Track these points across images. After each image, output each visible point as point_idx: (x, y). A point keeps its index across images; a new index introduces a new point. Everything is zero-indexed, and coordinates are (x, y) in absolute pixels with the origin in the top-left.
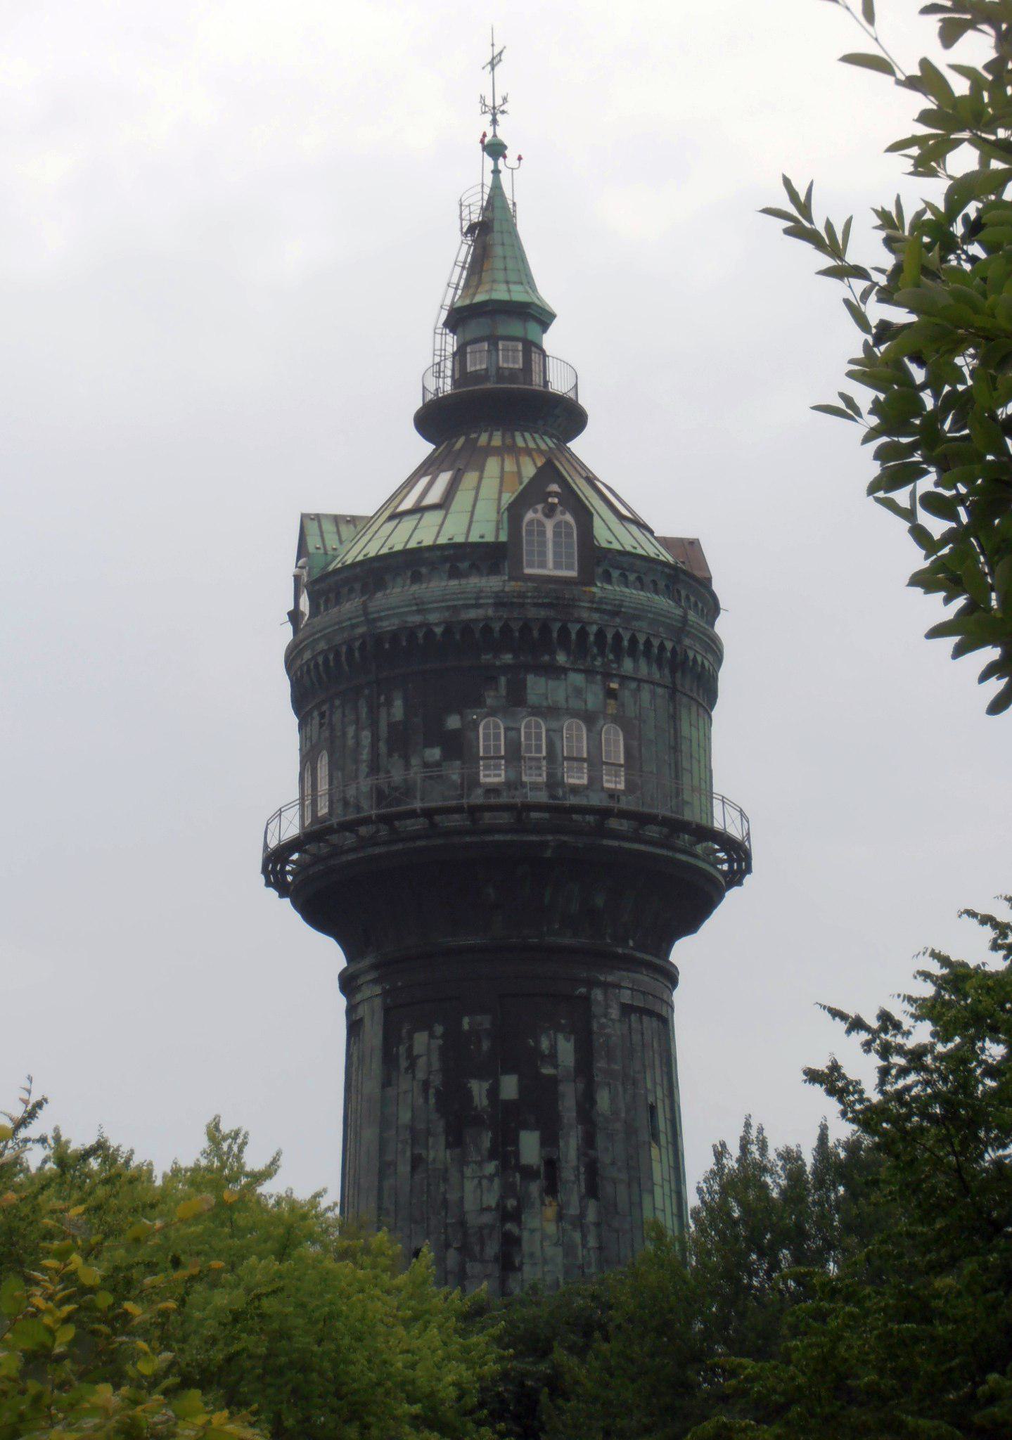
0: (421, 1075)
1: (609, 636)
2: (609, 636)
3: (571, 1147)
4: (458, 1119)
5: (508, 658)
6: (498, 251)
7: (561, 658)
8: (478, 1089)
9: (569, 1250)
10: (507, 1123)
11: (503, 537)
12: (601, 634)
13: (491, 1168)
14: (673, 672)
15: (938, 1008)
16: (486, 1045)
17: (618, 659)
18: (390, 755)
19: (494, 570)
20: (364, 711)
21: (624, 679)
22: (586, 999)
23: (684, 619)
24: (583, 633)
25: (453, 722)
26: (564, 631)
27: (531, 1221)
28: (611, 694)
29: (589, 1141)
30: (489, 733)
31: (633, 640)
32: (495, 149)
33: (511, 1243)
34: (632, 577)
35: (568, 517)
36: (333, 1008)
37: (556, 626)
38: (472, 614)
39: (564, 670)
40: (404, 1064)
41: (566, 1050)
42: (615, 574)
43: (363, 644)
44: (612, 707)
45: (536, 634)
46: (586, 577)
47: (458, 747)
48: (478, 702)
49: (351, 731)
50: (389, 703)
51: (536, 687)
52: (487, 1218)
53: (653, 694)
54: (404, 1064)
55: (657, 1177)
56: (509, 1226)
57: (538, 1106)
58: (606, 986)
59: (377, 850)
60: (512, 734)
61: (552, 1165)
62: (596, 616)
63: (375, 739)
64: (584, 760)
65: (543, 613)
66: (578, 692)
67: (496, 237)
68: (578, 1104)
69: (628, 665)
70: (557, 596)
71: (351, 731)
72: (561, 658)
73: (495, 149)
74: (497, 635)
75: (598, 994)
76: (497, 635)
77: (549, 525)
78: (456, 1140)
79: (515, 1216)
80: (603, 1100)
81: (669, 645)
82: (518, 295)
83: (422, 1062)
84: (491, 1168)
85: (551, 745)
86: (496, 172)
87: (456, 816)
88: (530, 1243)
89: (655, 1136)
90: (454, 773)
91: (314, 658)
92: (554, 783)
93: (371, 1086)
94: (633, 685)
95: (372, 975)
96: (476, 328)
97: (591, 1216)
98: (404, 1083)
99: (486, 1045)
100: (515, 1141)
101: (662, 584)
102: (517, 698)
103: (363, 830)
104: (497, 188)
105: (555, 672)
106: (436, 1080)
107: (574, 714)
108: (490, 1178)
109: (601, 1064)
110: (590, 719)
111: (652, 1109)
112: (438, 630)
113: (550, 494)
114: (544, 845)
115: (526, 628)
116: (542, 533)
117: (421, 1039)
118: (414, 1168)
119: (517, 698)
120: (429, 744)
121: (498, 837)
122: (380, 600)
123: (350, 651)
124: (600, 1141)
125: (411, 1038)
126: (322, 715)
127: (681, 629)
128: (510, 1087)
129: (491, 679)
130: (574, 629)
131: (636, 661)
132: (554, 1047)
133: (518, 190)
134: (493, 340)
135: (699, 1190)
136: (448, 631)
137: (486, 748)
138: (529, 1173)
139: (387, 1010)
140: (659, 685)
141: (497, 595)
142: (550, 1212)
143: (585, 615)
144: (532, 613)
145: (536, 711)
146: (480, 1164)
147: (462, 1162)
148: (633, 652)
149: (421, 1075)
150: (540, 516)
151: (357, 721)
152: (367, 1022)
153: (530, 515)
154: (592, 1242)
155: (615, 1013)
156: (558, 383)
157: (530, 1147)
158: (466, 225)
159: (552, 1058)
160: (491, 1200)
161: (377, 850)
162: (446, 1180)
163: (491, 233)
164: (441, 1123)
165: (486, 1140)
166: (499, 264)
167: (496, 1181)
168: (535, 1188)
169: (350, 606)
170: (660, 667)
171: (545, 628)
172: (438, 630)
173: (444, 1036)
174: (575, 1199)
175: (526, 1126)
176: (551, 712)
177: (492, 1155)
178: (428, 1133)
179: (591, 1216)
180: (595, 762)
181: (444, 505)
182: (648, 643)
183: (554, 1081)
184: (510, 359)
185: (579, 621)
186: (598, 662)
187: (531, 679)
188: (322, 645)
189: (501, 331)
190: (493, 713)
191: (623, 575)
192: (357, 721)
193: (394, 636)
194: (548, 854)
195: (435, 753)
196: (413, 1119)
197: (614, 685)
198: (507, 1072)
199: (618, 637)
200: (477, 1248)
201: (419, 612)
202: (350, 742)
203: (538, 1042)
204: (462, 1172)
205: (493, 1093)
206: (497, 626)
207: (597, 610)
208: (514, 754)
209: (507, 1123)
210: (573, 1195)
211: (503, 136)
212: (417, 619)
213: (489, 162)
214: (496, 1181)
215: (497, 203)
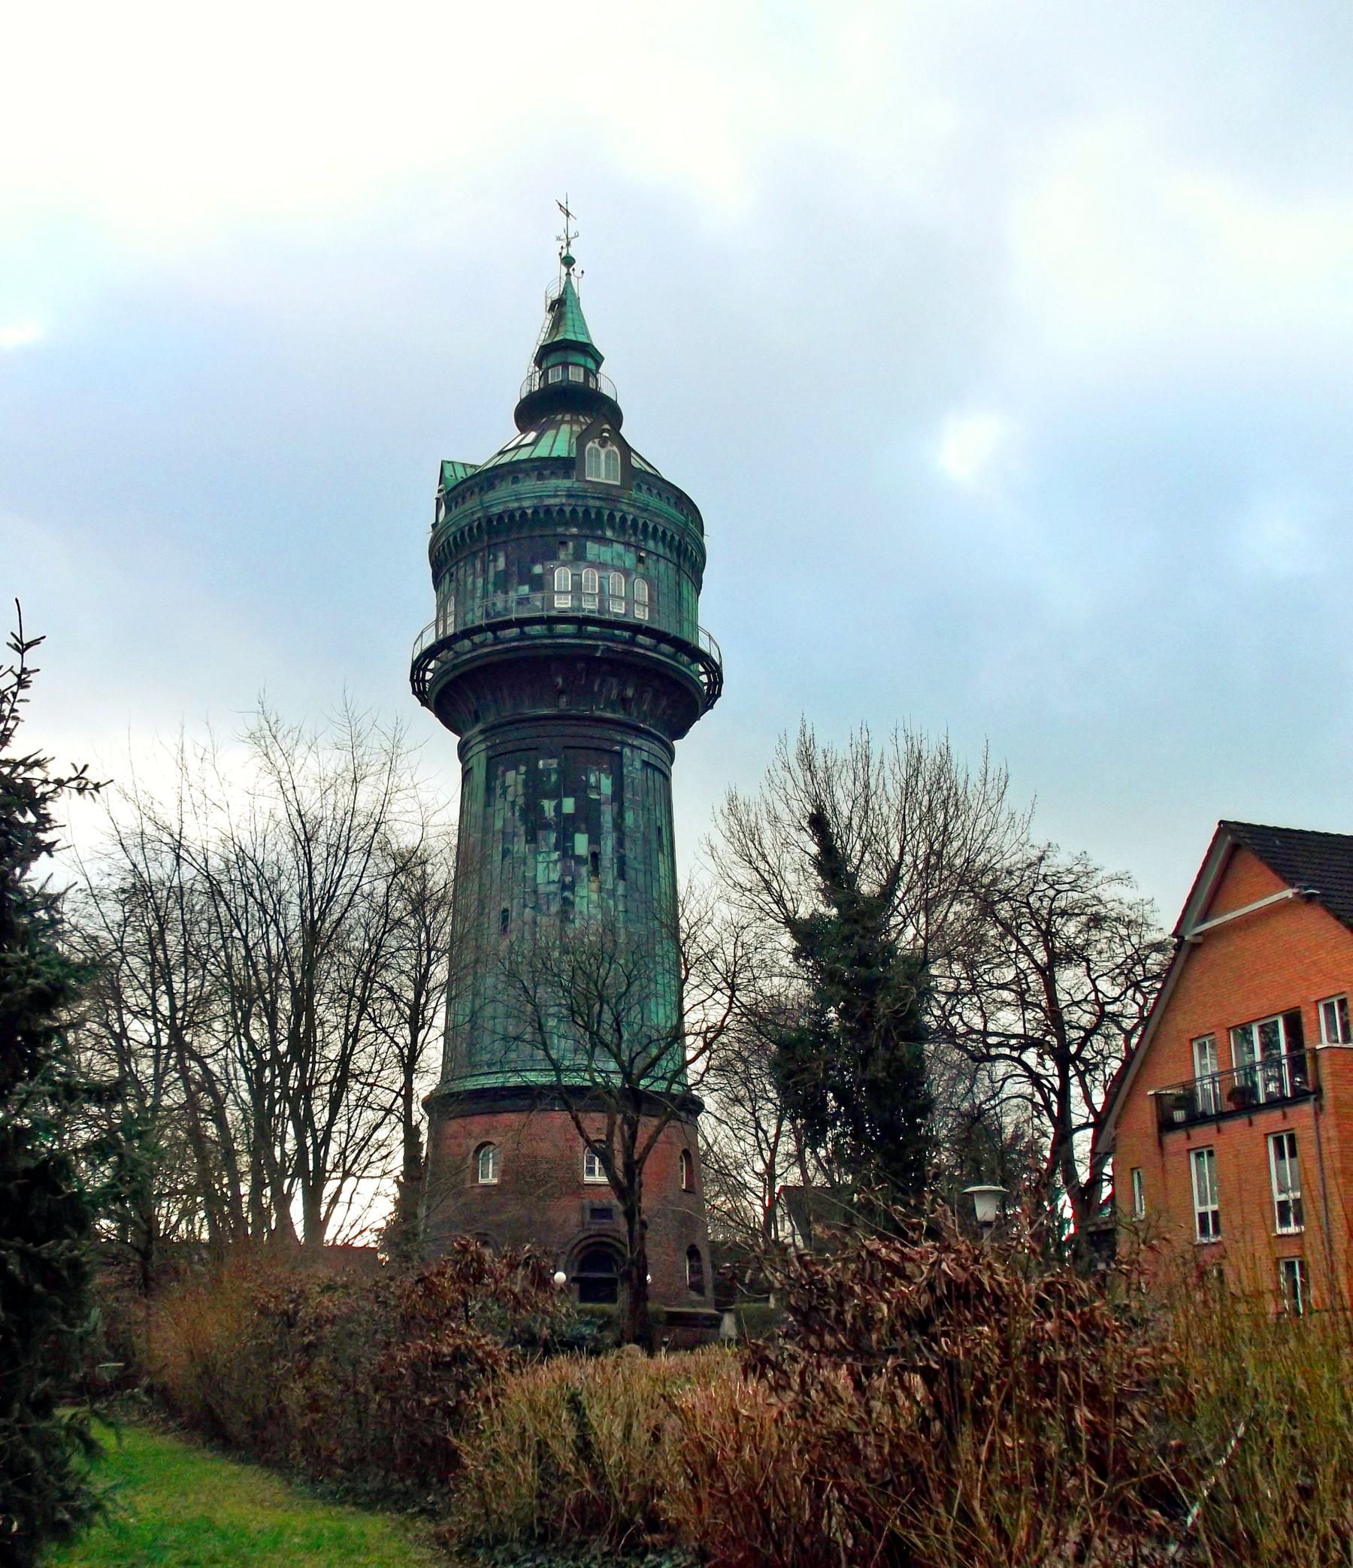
0: (510, 798)
1: (640, 522)
2: (640, 522)
3: (608, 845)
4: (534, 824)
6: (569, 315)
7: (609, 534)
8: (549, 806)
9: (605, 912)
10: (566, 828)
11: (573, 455)
12: (635, 521)
13: (555, 856)
14: (679, 556)
16: (554, 778)
17: (645, 539)
18: (495, 592)
19: (567, 475)
20: (479, 566)
21: (649, 552)
22: (620, 754)
23: (687, 524)
24: (623, 519)
25: (538, 569)
26: (611, 516)
27: (581, 891)
28: (640, 560)
29: (620, 843)
30: (562, 577)
31: (655, 529)
32: (568, 261)
33: (567, 903)
34: (655, 491)
35: (615, 449)
36: (454, 769)
37: (606, 513)
39: (611, 541)
40: (499, 791)
41: (606, 785)
42: (644, 487)
43: (479, 525)
44: (641, 568)
47: (539, 584)
48: (554, 557)
49: (470, 580)
50: (495, 560)
51: (592, 549)
52: (552, 888)
53: (667, 567)
55: (662, 872)
56: (566, 894)
57: (587, 818)
58: (632, 746)
59: (486, 650)
61: (595, 856)
62: (632, 510)
63: (486, 582)
64: (621, 598)
65: (598, 503)
66: (620, 556)
67: (568, 309)
68: (614, 820)
69: (651, 545)
70: (607, 494)
71: (470, 580)
72: (609, 534)
73: (568, 261)
74: (568, 515)
75: (627, 751)
76: (568, 515)
78: (532, 838)
79: (571, 887)
80: (629, 818)
81: (677, 538)
82: (582, 339)
83: (511, 790)
84: (555, 856)
85: (601, 586)
86: (568, 274)
87: (538, 627)
88: (581, 905)
89: (661, 845)
91: (448, 540)
93: (477, 807)
96: (552, 359)
97: (620, 891)
98: (499, 803)
99: (554, 778)
100: (572, 840)
101: (672, 501)
102: (579, 556)
103: (477, 639)
104: (568, 286)
105: (602, 540)
106: (521, 801)
107: (616, 569)
108: (555, 862)
109: (628, 795)
110: (626, 573)
111: (659, 830)
112: (529, 511)
113: (605, 430)
114: (597, 646)
116: (598, 456)
117: (511, 775)
118: (503, 857)
119: (579, 556)
120: (521, 583)
121: (566, 641)
122: (489, 496)
123: (471, 529)
124: (628, 844)
125: (504, 774)
126: (451, 575)
127: (684, 531)
128: (569, 805)
130: (618, 515)
131: (656, 543)
132: (598, 781)
133: (583, 289)
134: (565, 365)
135: (747, 840)
136: (536, 512)
137: (559, 585)
138: (580, 860)
139: (489, 759)
140: (476, 973)
141: (568, 489)
142: (594, 886)
143: (625, 508)
144: (591, 502)
145: (592, 565)
146: (548, 853)
147: (536, 852)
148: (654, 537)
149: (510, 798)
150: (597, 445)
151: (474, 574)
152: (475, 769)
153: (590, 445)
154: (621, 908)
155: (638, 764)
156: (606, 389)
157: (581, 844)
158: (549, 302)
159: (597, 788)
160: (555, 876)
161: (486, 650)
162: (525, 864)
163: (561, 307)
164: (523, 828)
165: (553, 838)
166: (569, 323)
167: (559, 866)
168: (584, 870)
169: (471, 503)
171: (599, 513)
172: (529, 511)
173: (526, 773)
174: (610, 879)
175: (578, 830)
176: (601, 566)
177: (556, 848)
178: (514, 834)
179: (620, 891)
180: (630, 601)
181: (534, 443)
183: (598, 802)
184: (576, 375)
187: (589, 544)
188: (453, 529)
189: (570, 359)
190: (563, 565)
192: (474, 574)
194: (598, 654)
195: (525, 589)
196: (504, 826)
198: (567, 795)
199: (645, 525)
200: (545, 907)
201: (517, 500)
202: (469, 587)
203: (588, 778)
204: (535, 859)
205: (558, 808)
206: (568, 509)
207: (633, 506)
208: (577, 588)
209: (566, 828)
210: (609, 876)
211: (572, 253)
212: (516, 505)
213: (564, 270)
214: (559, 866)
215: (569, 290)
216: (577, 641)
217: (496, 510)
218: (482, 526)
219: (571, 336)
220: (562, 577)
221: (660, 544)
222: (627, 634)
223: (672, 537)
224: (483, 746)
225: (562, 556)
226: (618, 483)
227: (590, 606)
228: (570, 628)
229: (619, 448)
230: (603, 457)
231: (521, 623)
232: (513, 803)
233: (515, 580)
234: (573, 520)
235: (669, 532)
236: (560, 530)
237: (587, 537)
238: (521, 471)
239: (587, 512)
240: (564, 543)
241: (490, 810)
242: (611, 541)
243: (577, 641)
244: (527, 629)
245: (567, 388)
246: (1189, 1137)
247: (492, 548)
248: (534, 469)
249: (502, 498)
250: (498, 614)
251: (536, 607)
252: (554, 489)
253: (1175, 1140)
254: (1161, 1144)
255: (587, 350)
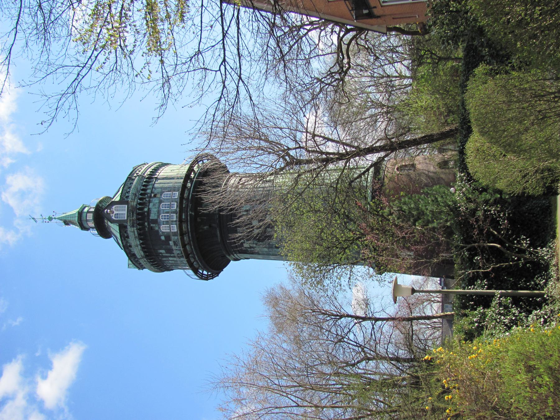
0: (255, 245)
1: (141, 196)
2: (141, 196)
5: (146, 224)
6: (69, 219)
7: (146, 209)
12: (140, 199)
15: (515, 182)
17: (147, 194)
20: (164, 259)
21: (152, 192)
24: (140, 204)
25: (163, 238)
26: (139, 209)
30: (164, 229)
31: (143, 190)
32: (50, 219)
34: (128, 190)
35: (114, 207)
38: (136, 233)
39: (149, 209)
40: (252, 249)
42: (127, 195)
44: (158, 196)
45: (140, 217)
46: (127, 203)
47: (168, 237)
48: (157, 231)
50: (161, 253)
51: (153, 216)
54: (252, 249)
60: (164, 223)
66: (154, 205)
69: (149, 191)
72: (146, 209)
73: (50, 219)
77: (115, 212)
82: (77, 215)
83: (251, 245)
86: (55, 218)
87: (185, 238)
90: (174, 238)
92: (175, 212)
94: (154, 189)
95: (232, 256)
96: (85, 225)
101: (131, 182)
103: (192, 260)
105: (149, 211)
110: (161, 202)
112: (141, 242)
114: (190, 215)
115: (138, 219)
119: (156, 221)
120: (169, 244)
129: (152, 229)
130: (138, 206)
134: (87, 220)
143: (135, 203)
144: (135, 218)
145: (158, 216)
149: (255, 245)
150: (113, 215)
153: (113, 218)
166: (72, 219)
169: (142, 261)
170: (150, 182)
171: (138, 214)
172: (141, 242)
176: (159, 212)
178: (269, 244)
182: (144, 186)
184: (90, 217)
185: (136, 205)
186: (147, 199)
187: (151, 218)
189: (85, 219)
190: (159, 228)
191: (127, 192)
193: (144, 252)
194: (193, 214)
195: (171, 243)
197: (153, 195)
206: (138, 227)
207: (134, 200)
212: (139, 246)
216: (189, 223)
217: (142, 254)
218: (150, 252)
219: (77, 218)
220: (164, 229)
221: (148, 187)
222: (184, 202)
223: (145, 182)
224: (235, 255)
225: (157, 229)
226: (126, 206)
227: (175, 217)
228: (184, 226)
229: (113, 206)
230: (117, 212)
231: (184, 246)
232: (256, 244)
233: (168, 246)
234: (142, 224)
235: (141, 191)
236: (147, 229)
237: (149, 218)
238: (126, 244)
239: (138, 219)
240: (152, 227)
241: (260, 252)
242: (149, 209)
243: (189, 223)
244: (186, 243)
245: (99, 220)
246: (375, 7)
247: (158, 255)
248: (125, 239)
249: (138, 252)
250: (182, 253)
251: (177, 238)
252: (132, 232)
253: (376, 12)
254: (378, 17)
255: (80, 214)
